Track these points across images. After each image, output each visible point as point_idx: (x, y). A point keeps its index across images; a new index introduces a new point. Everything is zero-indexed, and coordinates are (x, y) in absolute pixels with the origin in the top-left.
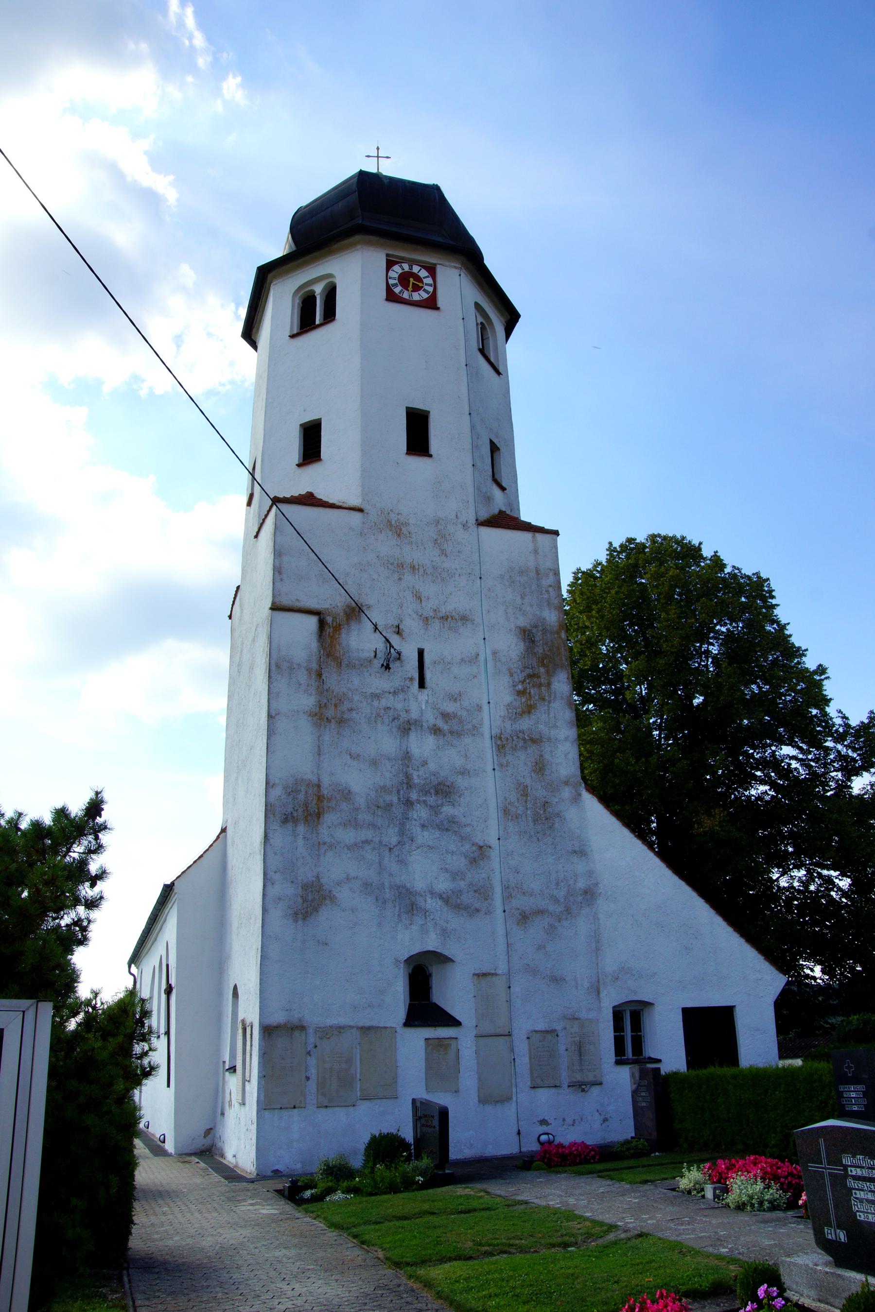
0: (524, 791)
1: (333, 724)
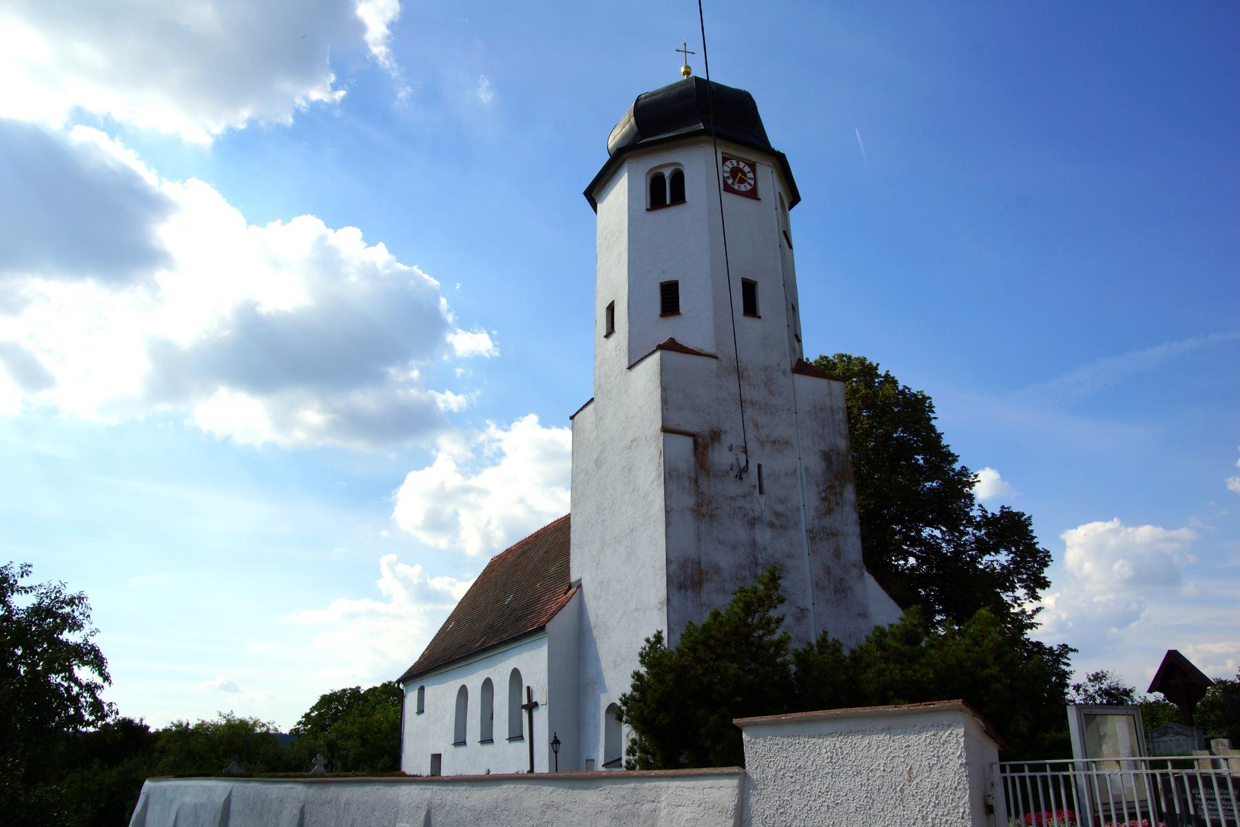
0: (828, 571)
1: (707, 518)
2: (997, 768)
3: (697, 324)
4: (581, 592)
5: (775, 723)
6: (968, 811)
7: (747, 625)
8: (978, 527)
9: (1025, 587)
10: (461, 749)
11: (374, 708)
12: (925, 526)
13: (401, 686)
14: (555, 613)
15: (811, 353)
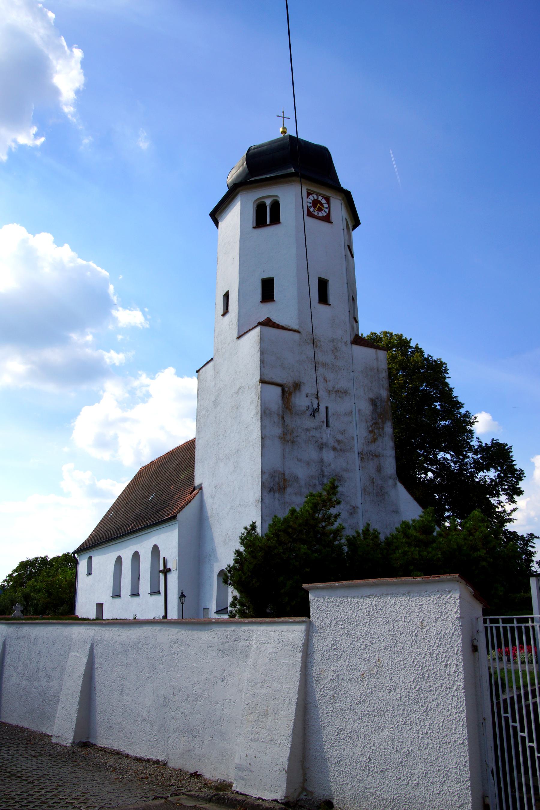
1: (290, 443)
2: (481, 621)
3: (286, 308)
4: (202, 492)
5: (331, 588)
6: (460, 649)
7: (314, 519)
8: (476, 452)
9: (506, 494)
10: (117, 600)
11: (57, 570)
12: (440, 451)
13: (76, 556)
14: (183, 507)
15: (365, 331)
